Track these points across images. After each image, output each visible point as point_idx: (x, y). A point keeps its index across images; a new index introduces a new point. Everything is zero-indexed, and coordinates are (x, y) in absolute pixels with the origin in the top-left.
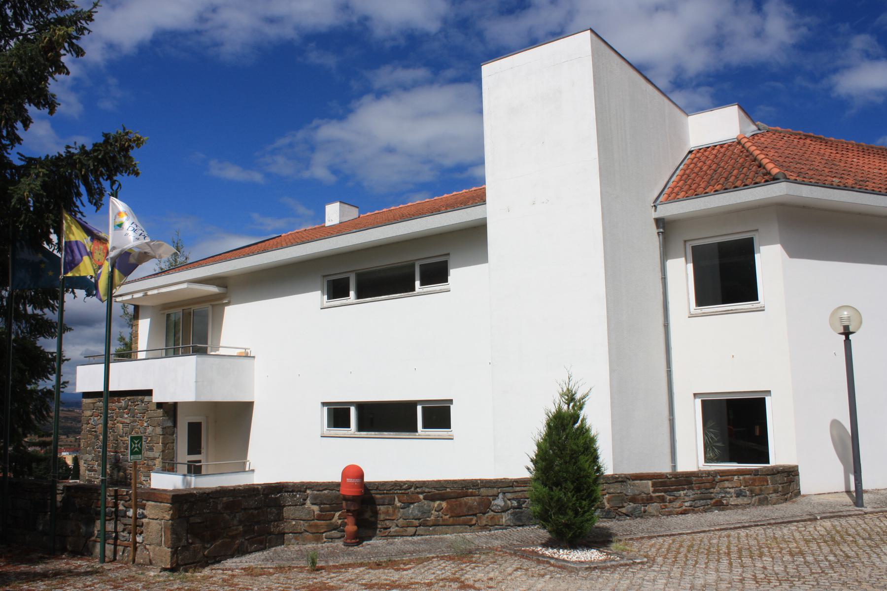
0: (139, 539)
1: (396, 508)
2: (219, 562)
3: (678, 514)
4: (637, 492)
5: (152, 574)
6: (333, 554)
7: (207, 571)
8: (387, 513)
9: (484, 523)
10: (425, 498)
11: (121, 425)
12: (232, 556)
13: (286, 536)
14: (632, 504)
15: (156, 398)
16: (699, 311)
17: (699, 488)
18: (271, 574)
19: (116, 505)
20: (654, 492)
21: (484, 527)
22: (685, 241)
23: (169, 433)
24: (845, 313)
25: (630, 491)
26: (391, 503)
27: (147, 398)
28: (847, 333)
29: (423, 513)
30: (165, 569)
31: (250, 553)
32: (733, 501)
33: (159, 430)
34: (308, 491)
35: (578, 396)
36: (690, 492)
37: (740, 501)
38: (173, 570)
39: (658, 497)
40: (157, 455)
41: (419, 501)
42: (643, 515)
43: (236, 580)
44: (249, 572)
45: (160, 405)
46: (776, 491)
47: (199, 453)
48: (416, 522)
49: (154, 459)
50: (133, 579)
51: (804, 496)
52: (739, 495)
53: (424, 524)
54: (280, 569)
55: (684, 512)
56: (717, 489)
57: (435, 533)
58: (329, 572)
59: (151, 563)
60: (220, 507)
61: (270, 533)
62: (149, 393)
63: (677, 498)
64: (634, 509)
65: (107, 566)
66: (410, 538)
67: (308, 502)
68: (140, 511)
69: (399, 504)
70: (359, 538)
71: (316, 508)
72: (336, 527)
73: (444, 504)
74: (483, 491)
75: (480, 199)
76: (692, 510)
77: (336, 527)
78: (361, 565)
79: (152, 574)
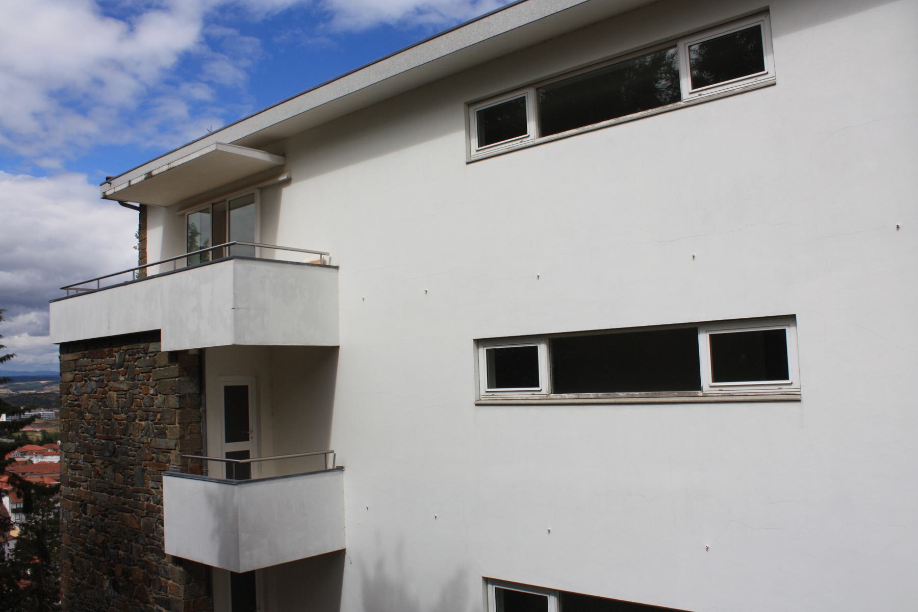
11: (114, 394)
15: (168, 344)
22: (685, 44)
27: (152, 347)
33: (173, 401)
40: (172, 444)
47: (246, 438)
49: (168, 450)
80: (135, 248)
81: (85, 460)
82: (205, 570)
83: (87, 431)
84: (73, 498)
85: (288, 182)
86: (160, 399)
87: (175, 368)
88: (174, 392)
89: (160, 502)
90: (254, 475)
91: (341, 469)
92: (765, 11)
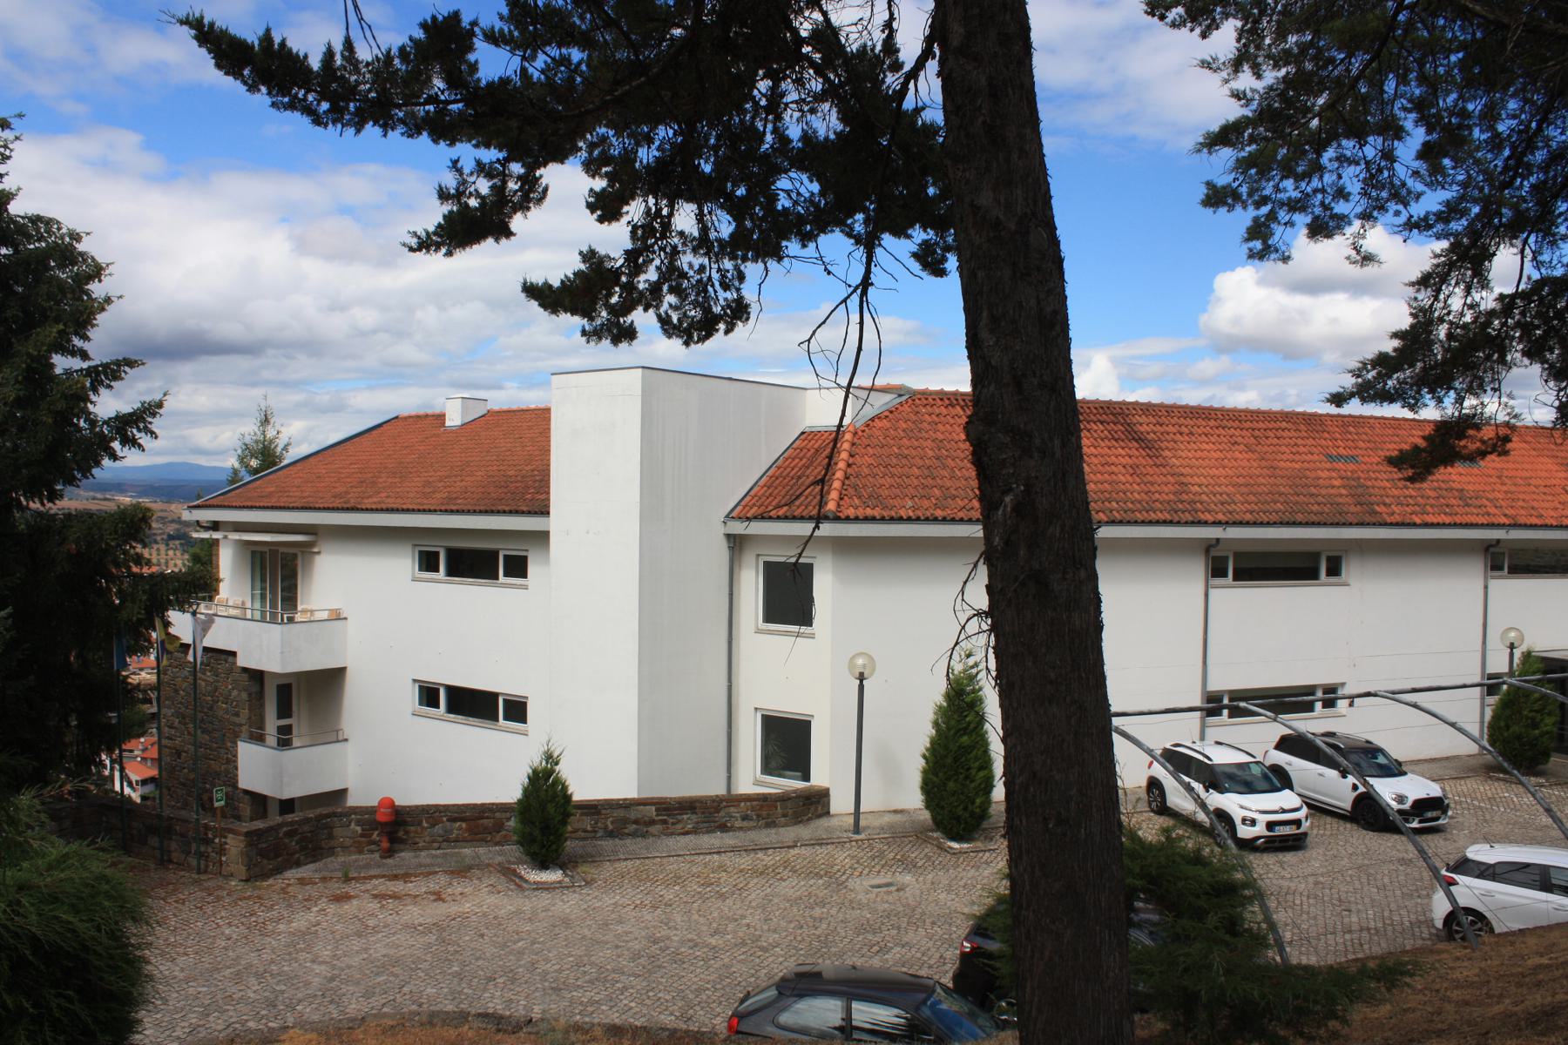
0: (224, 859)
1: (423, 828)
2: (281, 873)
3: (679, 834)
4: (639, 816)
5: (233, 883)
6: (367, 866)
7: (271, 881)
8: (416, 832)
9: (498, 840)
10: (448, 820)
11: (203, 684)
12: (291, 868)
13: (336, 850)
14: (634, 826)
15: (241, 662)
16: (764, 628)
17: (703, 813)
18: (316, 883)
19: (206, 834)
20: (657, 815)
21: (497, 844)
22: (758, 555)
23: (258, 699)
24: (860, 661)
25: (633, 815)
26: (420, 823)
27: (231, 659)
28: (861, 678)
29: (446, 832)
30: (242, 880)
31: (306, 864)
32: (738, 824)
33: (244, 696)
34: (353, 816)
35: (555, 755)
36: (693, 817)
37: (745, 824)
38: (247, 881)
39: (661, 820)
40: (244, 722)
41: (443, 822)
42: (644, 835)
43: (290, 889)
44: (302, 882)
45: (245, 670)
46: (785, 816)
47: (290, 716)
48: (441, 839)
49: (241, 725)
50: (220, 888)
51: (833, 816)
52: (745, 818)
53: (447, 840)
54: (324, 879)
55: (687, 833)
56: (722, 813)
57: (455, 847)
58: (357, 882)
59: (232, 875)
60: (281, 835)
61: (323, 849)
62: (234, 654)
63: (679, 822)
64: (637, 830)
65: (203, 877)
66: (434, 852)
67: (353, 824)
68: (223, 840)
69: (425, 825)
70: (389, 853)
71: (359, 829)
72: (374, 843)
73: (464, 825)
74: (498, 815)
75: (545, 512)
76: (695, 831)
77: (374, 843)
78: (384, 876)
79: (233, 883)
80: (1215, 212)
81: (179, 722)
82: (264, 798)
83: (181, 703)
84: (169, 748)
85: (319, 553)
86: (235, 693)
87: (245, 676)
88: (245, 690)
89: (235, 756)
90: (295, 745)
91: (346, 740)
92: (1346, 551)
